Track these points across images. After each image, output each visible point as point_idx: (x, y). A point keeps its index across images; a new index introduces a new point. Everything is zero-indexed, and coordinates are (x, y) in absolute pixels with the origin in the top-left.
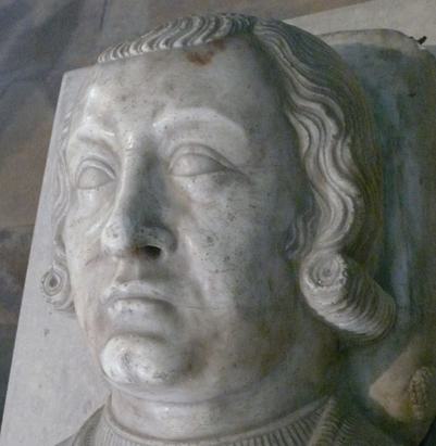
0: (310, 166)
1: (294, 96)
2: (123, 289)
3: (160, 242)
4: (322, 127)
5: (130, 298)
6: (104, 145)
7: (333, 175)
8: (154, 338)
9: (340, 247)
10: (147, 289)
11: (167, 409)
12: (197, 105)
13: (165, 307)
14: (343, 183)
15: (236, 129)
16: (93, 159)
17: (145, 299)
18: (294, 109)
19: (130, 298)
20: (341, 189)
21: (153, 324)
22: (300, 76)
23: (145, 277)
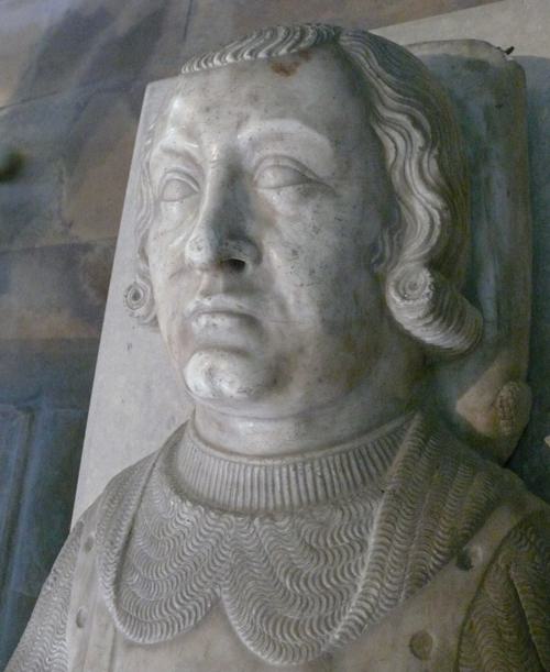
1: (380, 108)
2: (207, 303)
3: (245, 256)
4: (408, 138)
5: (214, 312)
8: (239, 352)
10: (231, 302)
12: (282, 116)
13: (249, 321)
14: (430, 196)
16: (177, 171)
17: (229, 313)
18: (380, 120)
19: (214, 312)
21: (238, 339)
23: (229, 290)
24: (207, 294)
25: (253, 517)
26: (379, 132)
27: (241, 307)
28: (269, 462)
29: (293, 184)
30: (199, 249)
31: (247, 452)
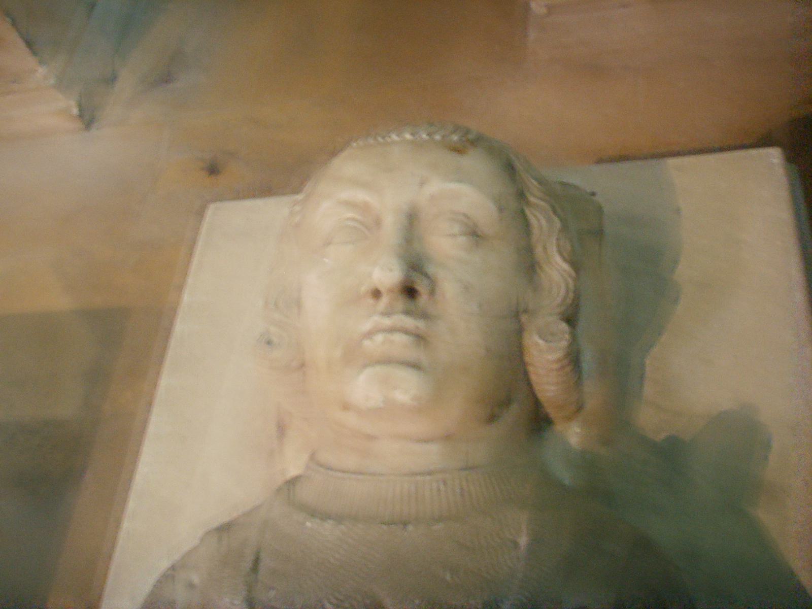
0: (539, 250)
1: (528, 195)
2: (387, 322)
3: (422, 287)
4: (549, 220)
5: (392, 330)
6: (365, 208)
7: (558, 259)
8: (415, 366)
9: (405, 289)
10: (409, 322)
11: (523, 541)
12: (460, 181)
13: (420, 338)
14: (566, 266)
15: (491, 207)
16: (353, 219)
17: (406, 332)
18: (528, 203)
19: (392, 330)
20: (565, 271)
21: (413, 354)
22: (533, 181)
23: (407, 313)
24: (387, 314)
25: (405, 524)
26: (527, 212)
27: (417, 328)
28: (419, 478)
29: (466, 234)
30: (391, 270)
31: (639, 163)
